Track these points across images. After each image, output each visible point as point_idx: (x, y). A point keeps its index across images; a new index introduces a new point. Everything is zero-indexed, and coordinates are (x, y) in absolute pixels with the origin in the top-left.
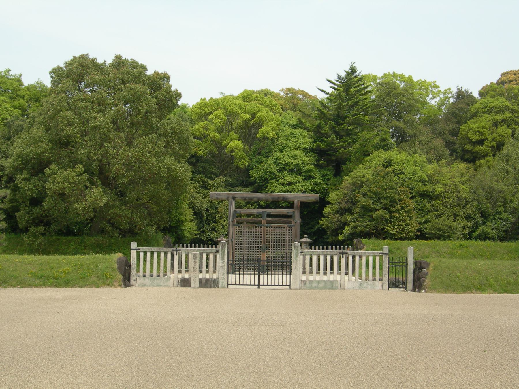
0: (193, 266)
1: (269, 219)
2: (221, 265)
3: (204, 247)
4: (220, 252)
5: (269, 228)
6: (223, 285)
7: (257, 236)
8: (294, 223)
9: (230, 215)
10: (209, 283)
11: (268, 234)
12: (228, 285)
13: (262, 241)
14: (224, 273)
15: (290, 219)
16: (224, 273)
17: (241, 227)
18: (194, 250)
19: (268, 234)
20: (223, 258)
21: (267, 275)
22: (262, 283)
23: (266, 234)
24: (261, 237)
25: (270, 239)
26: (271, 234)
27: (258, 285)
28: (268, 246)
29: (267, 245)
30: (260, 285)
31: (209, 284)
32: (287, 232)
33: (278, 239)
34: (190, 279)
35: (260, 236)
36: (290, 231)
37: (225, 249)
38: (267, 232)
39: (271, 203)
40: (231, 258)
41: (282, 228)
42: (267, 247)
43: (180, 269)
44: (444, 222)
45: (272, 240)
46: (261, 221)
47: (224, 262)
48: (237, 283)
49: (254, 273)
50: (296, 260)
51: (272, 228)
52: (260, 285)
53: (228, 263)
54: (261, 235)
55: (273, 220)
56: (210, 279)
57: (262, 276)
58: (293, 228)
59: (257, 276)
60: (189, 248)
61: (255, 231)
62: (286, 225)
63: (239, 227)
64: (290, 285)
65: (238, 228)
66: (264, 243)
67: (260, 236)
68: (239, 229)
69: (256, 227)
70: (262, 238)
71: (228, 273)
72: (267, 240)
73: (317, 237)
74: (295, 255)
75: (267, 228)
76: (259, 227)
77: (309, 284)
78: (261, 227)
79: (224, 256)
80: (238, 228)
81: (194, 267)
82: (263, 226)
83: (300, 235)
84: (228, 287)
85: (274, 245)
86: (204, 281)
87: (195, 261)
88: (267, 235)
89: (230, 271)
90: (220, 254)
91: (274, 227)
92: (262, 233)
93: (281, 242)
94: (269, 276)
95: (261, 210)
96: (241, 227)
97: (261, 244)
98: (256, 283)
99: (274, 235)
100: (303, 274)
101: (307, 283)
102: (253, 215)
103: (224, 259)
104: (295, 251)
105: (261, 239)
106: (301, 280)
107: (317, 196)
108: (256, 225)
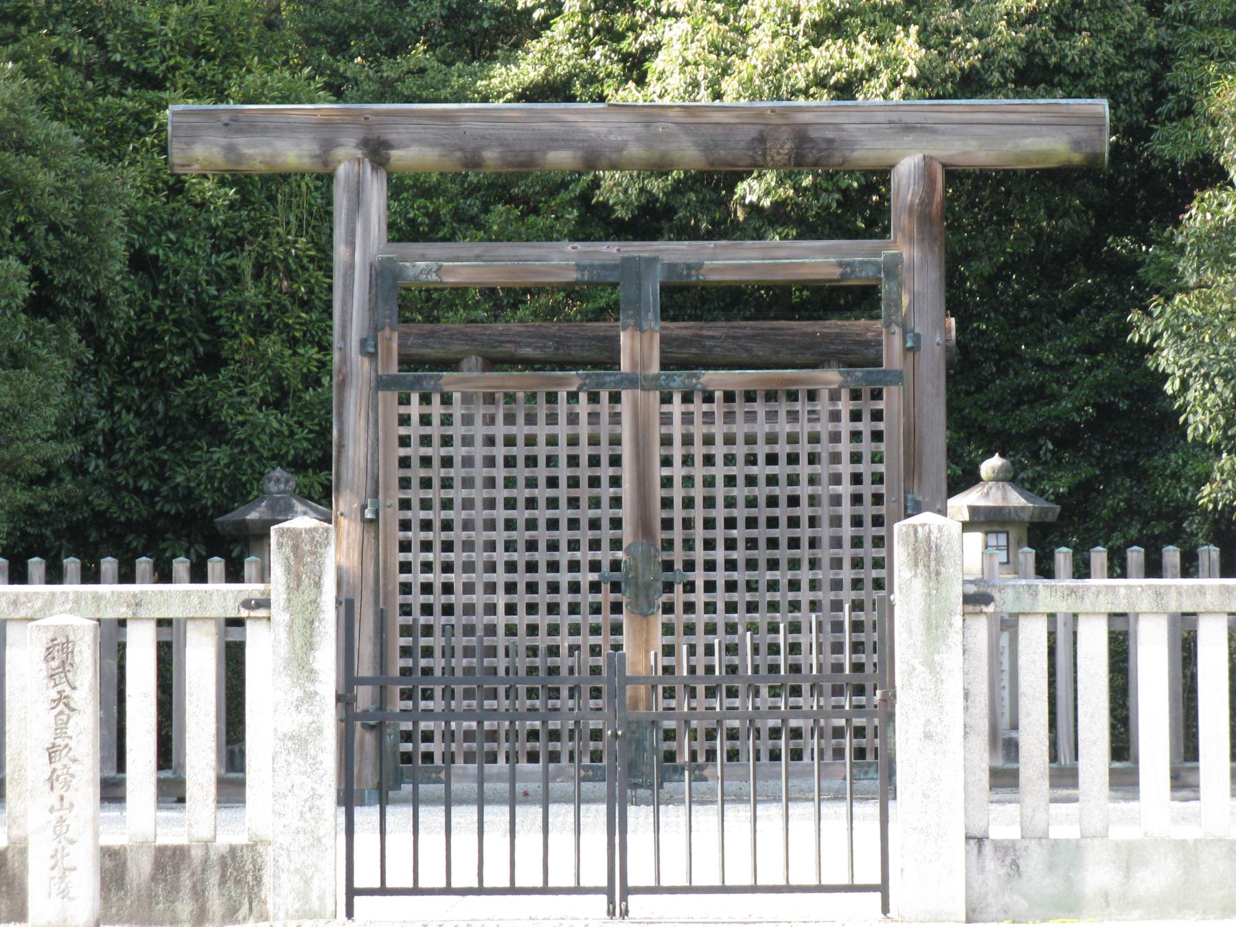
0: (48, 739)
1: (681, 329)
2: (292, 722)
3: (127, 576)
4: (278, 611)
5: (687, 398)
6: (304, 896)
7: (584, 472)
8: (893, 352)
9: (347, 302)
10: (186, 880)
11: (677, 452)
12: (352, 892)
13: (626, 513)
14: (314, 795)
15: (858, 326)
16: (314, 795)
17: (446, 400)
18: (50, 601)
19: (677, 452)
20: (301, 665)
21: (416, 803)
22: (639, 874)
23: (657, 452)
24: (616, 481)
25: (698, 493)
26: (698, 450)
27: (609, 891)
28: (678, 555)
29: (668, 545)
30: (627, 891)
31: (185, 893)
32: (835, 437)
33: (762, 491)
34: (23, 851)
35: (605, 472)
36: (865, 426)
37: (318, 585)
38: (667, 441)
39: (679, 188)
40: (365, 667)
41: (792, 396)
42: (668, 566)
43: (167, 774)
44: (455, 348)
45: (709, 502)
46: (612, 345)
47: (310, 696)
48: (432, 876)
49: (570, 787)
50: (932, 667)
51: (709, 398)
52: (627, 891)
53: (344, 699)
54: (616, 461)
55: (716, 330)
56: (197, 854)
57: (639, 817)
58: (892, 401)
59: (595, 815)
60: (1137, 582)
61: (562, 430)
62: (831, 376)
63: (426, 399)
64: (883, 888)
65: (415, 409)
66: (644, 528)
67: (605, 472)
68: (425, 420)
69: (573, 397)
70: (627, 491)
71: (348, 799)
72: (667, 503)
73: (1087, 471)
74: (919, 627)
75: (666, 399)
76: (594, 398)
77: (1051, 867)
78: (615, 398)
79: (310, 646)
80: (415, 409)
81: (52, 752)
82: (632, 382)
83: (953, 454)
84: (350, 913)
85: (731, 544)
86: (140, 869)
87: (62, 700)
88: (667, 462)
89: (367, 773)
90: (283, 634)
91: (729, 397)
92: (626, 451)
93: (426, 525)
94: (432, 817)
95: (610, 251)
96: (446, 400)
97: (616, 544)
98: (596, 875)
99: (772, 459)
100: (993, 786)
101: (1034, 861)
102: (537, 290)
103: (311, 674)
104: (918, 585)
105: (616, 502)
106: (980, 841)
107: (1093, 121)
108: (575, 378)
